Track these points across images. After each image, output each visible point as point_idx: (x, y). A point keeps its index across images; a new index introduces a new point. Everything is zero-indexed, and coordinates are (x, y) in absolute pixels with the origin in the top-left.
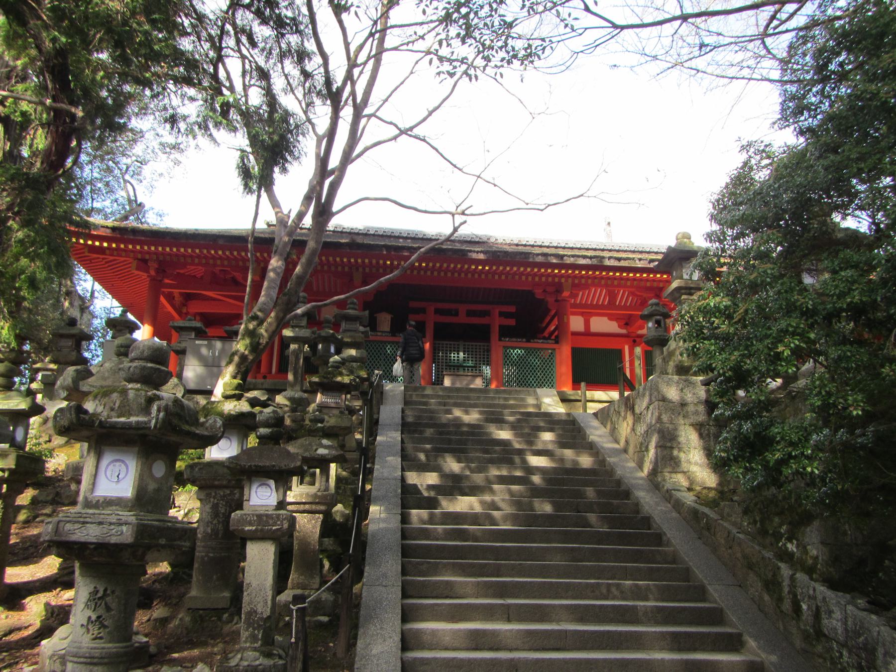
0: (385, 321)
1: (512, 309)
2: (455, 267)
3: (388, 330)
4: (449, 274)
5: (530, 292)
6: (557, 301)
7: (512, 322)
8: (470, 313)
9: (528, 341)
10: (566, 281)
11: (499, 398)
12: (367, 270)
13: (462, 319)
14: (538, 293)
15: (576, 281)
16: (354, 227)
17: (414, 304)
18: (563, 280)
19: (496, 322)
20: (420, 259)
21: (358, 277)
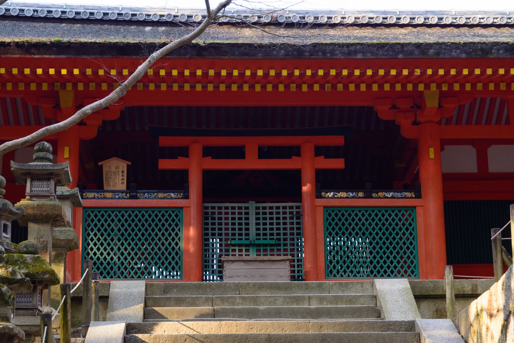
0: (116, 173)
1: (338, 140)
2: (314, 75)
3: (124, 187)
4: (293, 87)
5: (370, 108)
6: (416, 123)
7: (339, 164)
8: (264, 153)
9: (368, 196)
10: (427, 87)
11: (310, 298)
12: (81, 87)
13: (251, 162)
14: (384, 111)
15: (445, 88)
16: (264, 7)
17: (165, 141)
18: (421, 87)
19: (308, 166)
20: (156, 65)
21: (66, 99)
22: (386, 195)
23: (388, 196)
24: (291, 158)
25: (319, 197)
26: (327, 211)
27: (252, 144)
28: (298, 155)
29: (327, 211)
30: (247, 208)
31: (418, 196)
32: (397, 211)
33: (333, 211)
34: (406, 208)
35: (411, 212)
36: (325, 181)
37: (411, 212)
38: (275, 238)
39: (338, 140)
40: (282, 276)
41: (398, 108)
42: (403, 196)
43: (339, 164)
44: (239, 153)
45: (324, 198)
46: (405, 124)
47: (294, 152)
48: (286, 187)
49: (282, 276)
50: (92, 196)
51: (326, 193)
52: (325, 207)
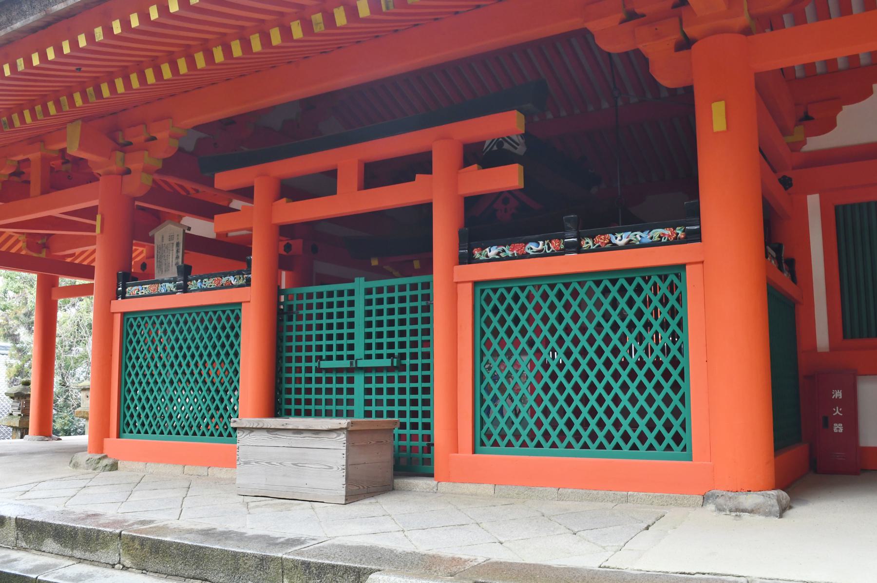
1: (509, 124)
7: (509, 178)
22: (614, 241)
23: (617, 242)
24: (413, 179)
25: (467, 259)
26: (482, 291)
27: (347, 160)
28: (427, 169)
29: (482, 291)
30: (351, 293)
31: (694, 236)
32: (639, 280)
33: (495, 291)
34: (663, 272)
35: (676, 281)
36: (485, 223)
37: (676, 281)
38: (396, 354)
39: (509, 124)
40: (331, 468)
41: (643, 15)
42: (656, 239)
43: (509, 178)
44: (325, 184)
45: (479, 261)
46: (658, 51)
47: (418, 165)
48: (400, 244)
49: (331, 468)
50: (625, 240)
51: (483, 248)
52: (475, 283)
